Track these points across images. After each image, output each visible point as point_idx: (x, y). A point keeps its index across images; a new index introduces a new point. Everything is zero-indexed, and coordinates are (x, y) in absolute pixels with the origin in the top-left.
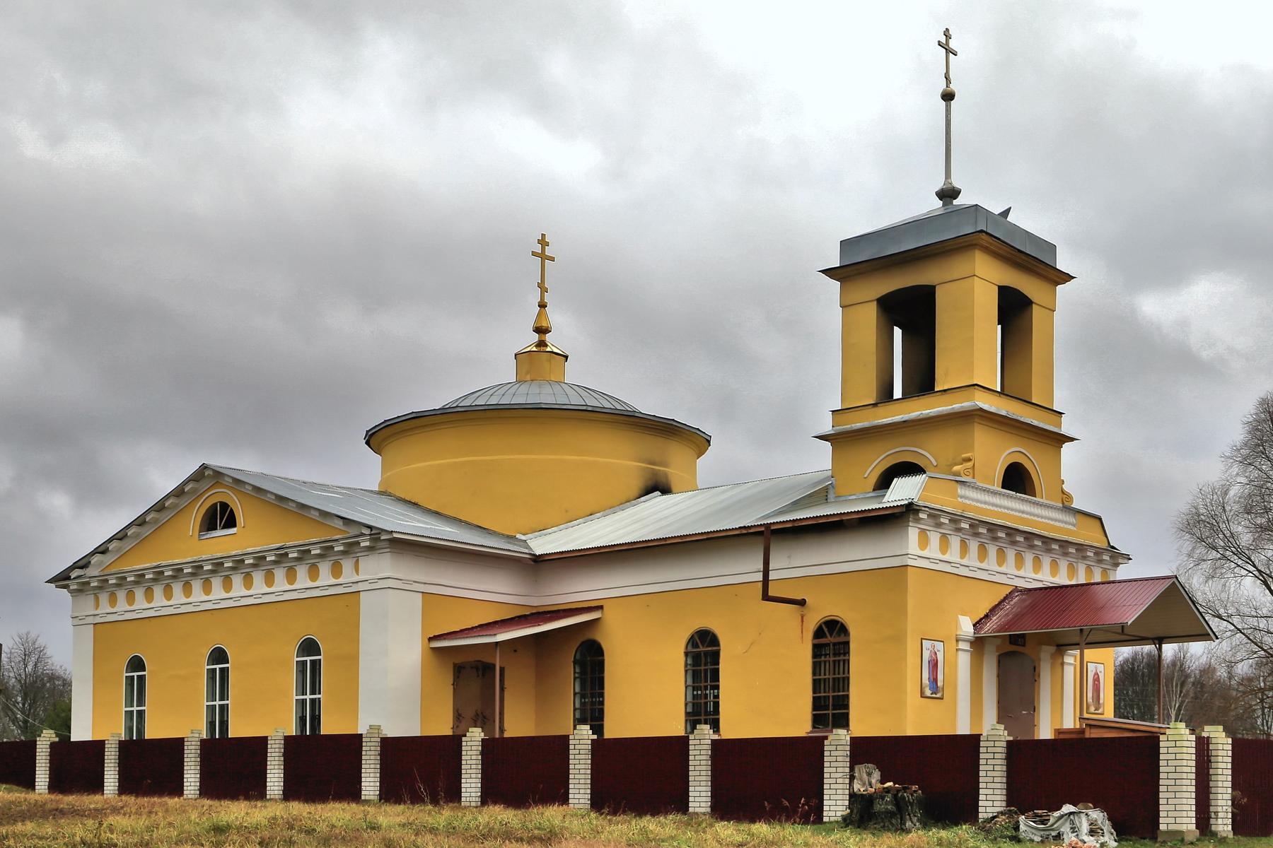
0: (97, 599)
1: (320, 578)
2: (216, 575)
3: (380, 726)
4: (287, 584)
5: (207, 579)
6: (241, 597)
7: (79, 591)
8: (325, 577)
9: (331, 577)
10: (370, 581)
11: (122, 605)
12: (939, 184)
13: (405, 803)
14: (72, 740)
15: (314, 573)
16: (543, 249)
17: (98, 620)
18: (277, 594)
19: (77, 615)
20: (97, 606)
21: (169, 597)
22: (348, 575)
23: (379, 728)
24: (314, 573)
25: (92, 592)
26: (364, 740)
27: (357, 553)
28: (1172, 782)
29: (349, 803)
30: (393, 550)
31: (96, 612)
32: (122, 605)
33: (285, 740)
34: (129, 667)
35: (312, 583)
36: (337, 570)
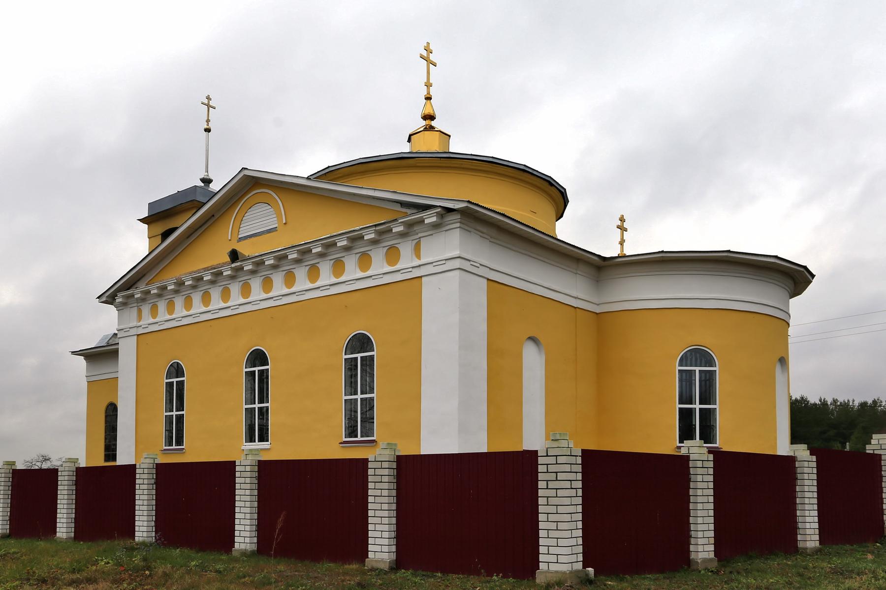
0: (140, 312)
1: (345, 273)
2: (197, 290)
3: (78, 459)
4: (263, 293)
5: (392, 247)
6: (219, 309)
7: (124, 304)
8: (379, 266)
9: (221, 301)
10: (232, 308)
11: (216, 302)
12: (202, 175)
13: (478, 574)
14: (806, 445)
15: (365, 261)
16: (428, 55)
17: (141, 331)
18: (434, 264)
19: (122, 327)
20: (140, 318)
21: (154, 317)
22: (407, 259)
23: (13, 463)
24: (365, 261)
25: (135, 305)
26: (238, 468)
27: (417, 234)
28: (553, 526)
29: (310, 562)
30: (462, 226)
31: (139, 324)
32: (198, 307)
33: (157, 469)
34: (249, 362)
35: (205, 308)
36: (393, 255)
